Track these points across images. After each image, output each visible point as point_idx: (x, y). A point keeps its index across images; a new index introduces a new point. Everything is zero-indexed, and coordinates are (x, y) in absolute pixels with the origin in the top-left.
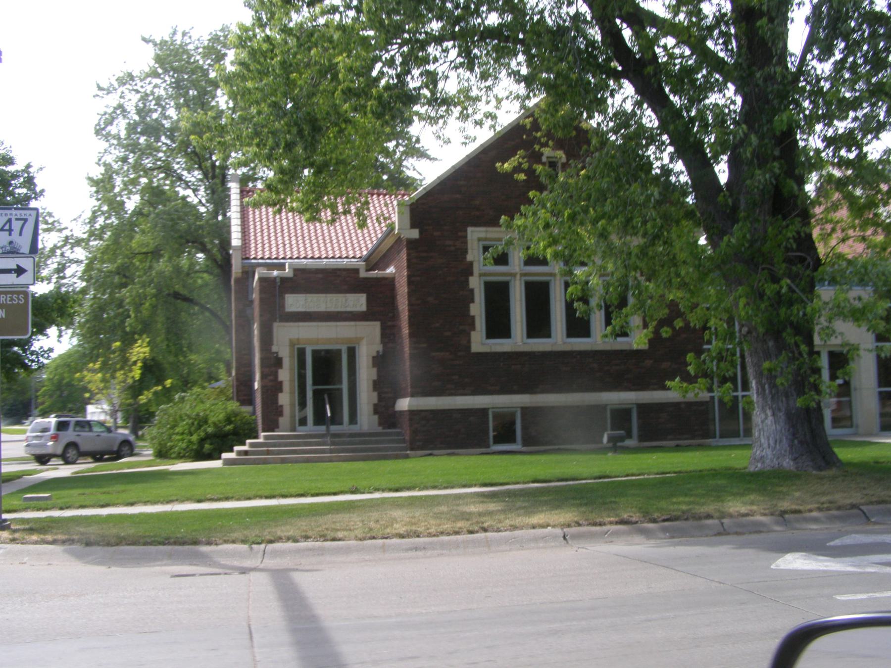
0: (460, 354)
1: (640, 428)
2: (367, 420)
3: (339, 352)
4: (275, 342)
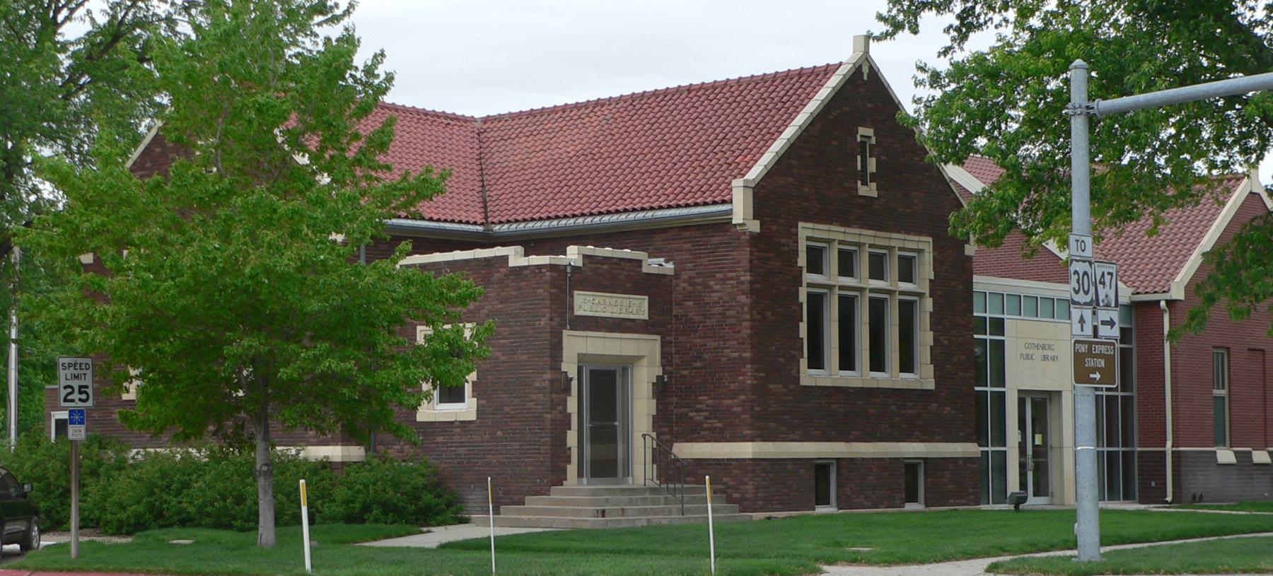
1: (838, 497)
2: (642, 469)
3: (614, 372)
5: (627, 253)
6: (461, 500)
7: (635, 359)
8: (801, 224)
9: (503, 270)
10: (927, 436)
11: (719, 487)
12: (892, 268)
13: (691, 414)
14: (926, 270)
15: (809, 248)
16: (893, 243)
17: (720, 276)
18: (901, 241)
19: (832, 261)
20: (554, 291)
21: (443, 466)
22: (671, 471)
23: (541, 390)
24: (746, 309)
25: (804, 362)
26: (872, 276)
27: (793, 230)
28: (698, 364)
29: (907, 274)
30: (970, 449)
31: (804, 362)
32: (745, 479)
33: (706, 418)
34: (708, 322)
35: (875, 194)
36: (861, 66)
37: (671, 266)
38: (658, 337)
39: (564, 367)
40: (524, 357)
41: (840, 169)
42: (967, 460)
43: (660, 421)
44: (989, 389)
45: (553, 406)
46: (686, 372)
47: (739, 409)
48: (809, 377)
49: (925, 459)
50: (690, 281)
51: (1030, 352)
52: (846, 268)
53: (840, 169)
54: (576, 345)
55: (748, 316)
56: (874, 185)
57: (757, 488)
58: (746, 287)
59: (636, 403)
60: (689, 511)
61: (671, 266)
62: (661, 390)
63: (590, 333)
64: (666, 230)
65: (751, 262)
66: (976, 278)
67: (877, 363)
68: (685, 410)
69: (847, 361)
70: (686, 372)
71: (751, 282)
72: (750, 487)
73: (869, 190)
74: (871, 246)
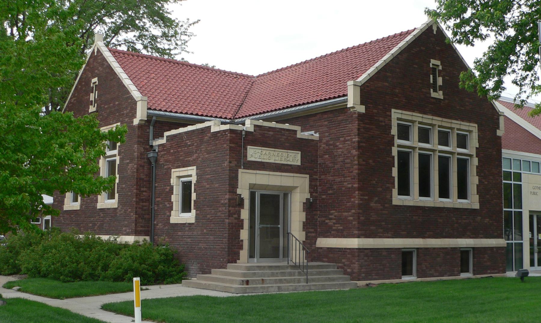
0: (386, 205)
1: (417, 271)
2: (297, 254)
3: (278, 196)
4: (239, 186)
5: (287, 126)
6: (187, 269)
7: (292, 189)
8: (393, 110)
9: (209, 135)
10: (475, 235)
11: (340, 265)
12: (453, 140)
13: (327, 221)
14: (474, 142)
15: (399, 125)
16: (453, 126)
17: (342, 139)
18: (458, 126)
19: (415, 133)
20: (233, 145)
21: (181, 249)
22: (314, 254)
23: (224, 205)
24: (355, 158)
25: (395, 191)
26: (440, 144)
27: (388, 113)
28: (330, 192)
29: (462, 142)
30: (501, 242)
31: (395, 191)
32: (354, 261)
33: (334, 224)
34: (336, 167)
35: (442, 97)
36: (431, 26)
37: (317, 135)
38: (308, 176)
39: (239, 191)
40: (217, 185)
41: (419, 81)
42: (499, 248)
43: (307, 226)
44: (513, 210)
45: (230, 215)
46: (324, 197)
47: (351, 218)
48: (398, 199)
49: (473, 248)
50: (327, 144)
51: (536, 191)
52: (424, 136)
53: (419, 81)
54: (246, 179)
55: (356, 162)
56: (441, 92)
57: (361, 266)
58: (356, 144)
59: (293, 213)
60: (313, 280)
61: (317, 135)
62: (309, 207)
63: (258, 172)
64: (315, 115)
65: (359, 129)
66: (503, 151)
67: (444, 193)
68: (323, 219)
69: (425, 191)
70: (324, 197)
71: (359, 142)
72: (356, 266)
73: (439, 95)
74: (439, 126)
